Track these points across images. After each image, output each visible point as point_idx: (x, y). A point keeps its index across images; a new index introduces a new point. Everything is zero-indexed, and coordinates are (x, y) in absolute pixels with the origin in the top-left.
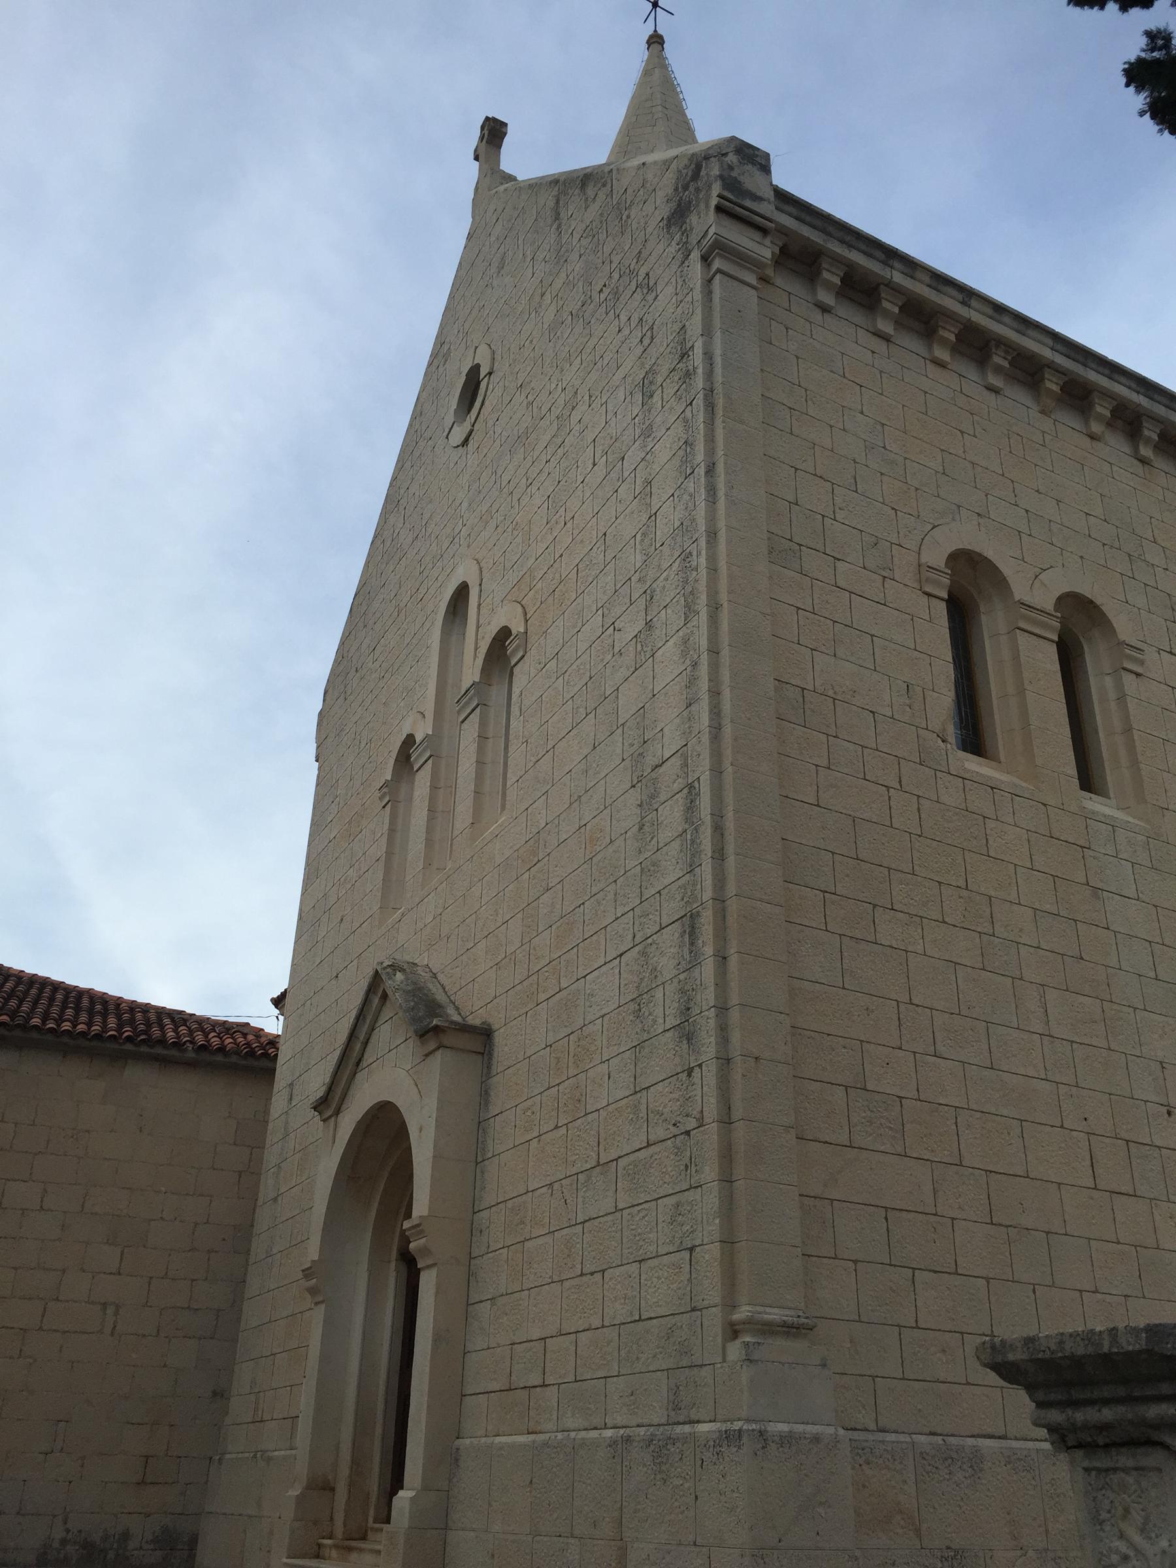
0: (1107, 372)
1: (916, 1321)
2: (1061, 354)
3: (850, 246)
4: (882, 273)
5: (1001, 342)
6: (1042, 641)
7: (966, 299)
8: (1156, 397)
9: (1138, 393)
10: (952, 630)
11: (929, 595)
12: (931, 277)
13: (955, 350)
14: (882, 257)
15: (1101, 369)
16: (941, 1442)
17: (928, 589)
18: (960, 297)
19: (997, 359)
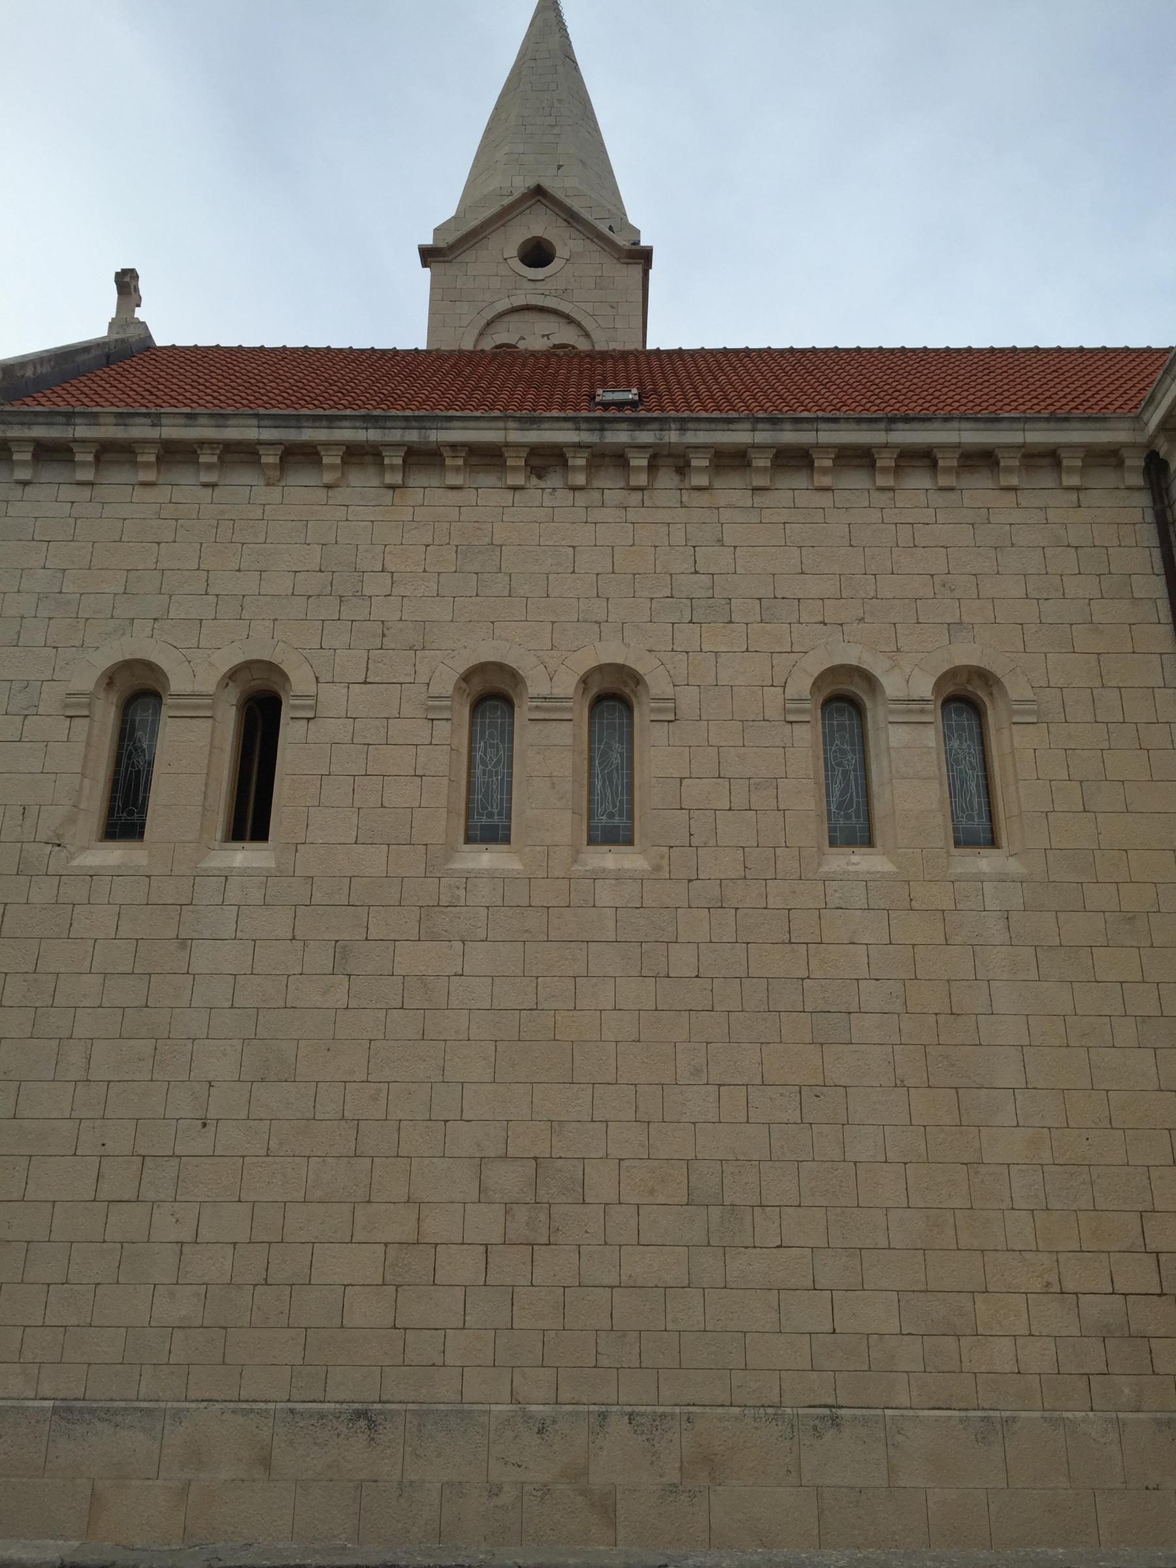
0: (325, 423)
1: (1015, 1341)
2: (351, 428)
3: (30, 425)
4: (64, 435)
5: (202, 443)
6: (195, 721)
7: (155, 421)
8: (389, 424)
9: (367, 428)
10: (469, 737)
11: (791, 722)
12: (115, 417)
13: (1083, 470)
14: (63, 420)
15: (317, 424)
16: (829, 1413)
17: (791, 718)
18: (148, 421)
19: (757, 463)
